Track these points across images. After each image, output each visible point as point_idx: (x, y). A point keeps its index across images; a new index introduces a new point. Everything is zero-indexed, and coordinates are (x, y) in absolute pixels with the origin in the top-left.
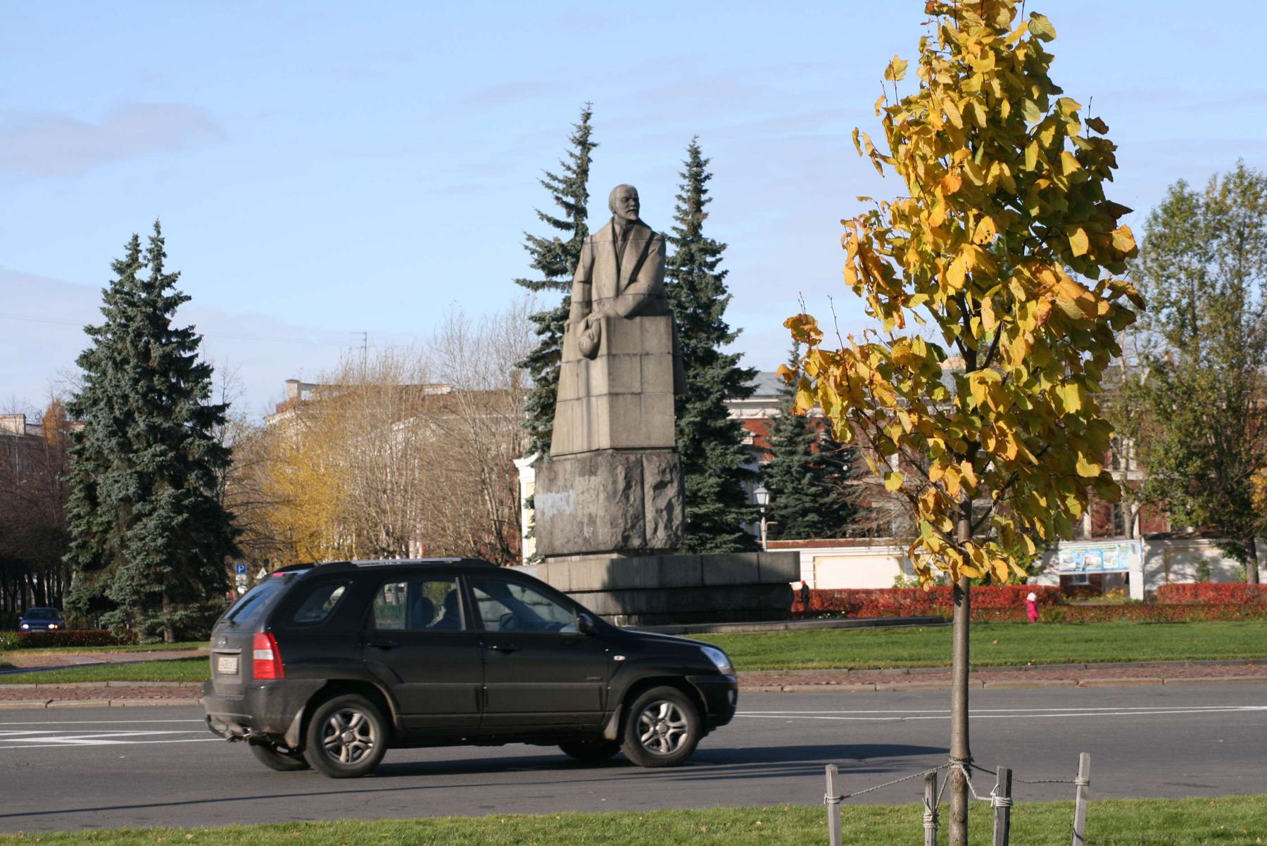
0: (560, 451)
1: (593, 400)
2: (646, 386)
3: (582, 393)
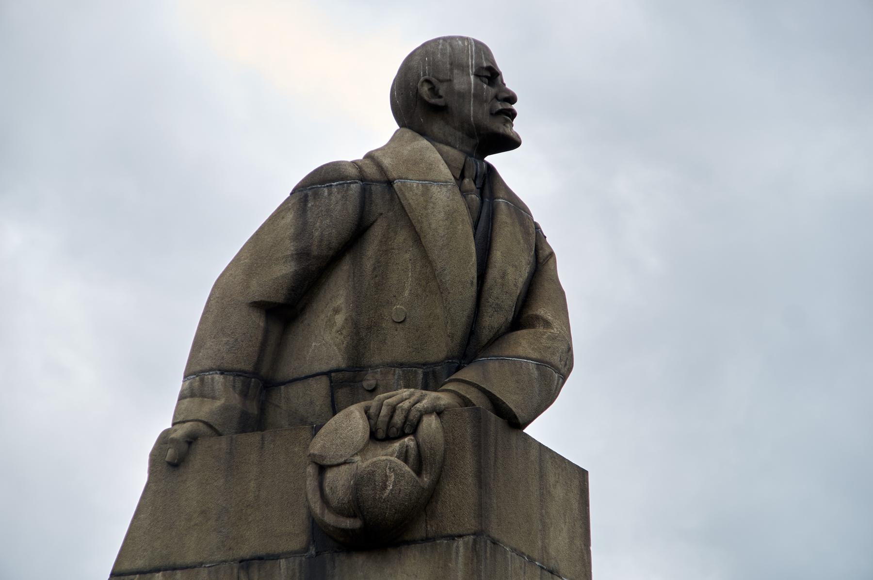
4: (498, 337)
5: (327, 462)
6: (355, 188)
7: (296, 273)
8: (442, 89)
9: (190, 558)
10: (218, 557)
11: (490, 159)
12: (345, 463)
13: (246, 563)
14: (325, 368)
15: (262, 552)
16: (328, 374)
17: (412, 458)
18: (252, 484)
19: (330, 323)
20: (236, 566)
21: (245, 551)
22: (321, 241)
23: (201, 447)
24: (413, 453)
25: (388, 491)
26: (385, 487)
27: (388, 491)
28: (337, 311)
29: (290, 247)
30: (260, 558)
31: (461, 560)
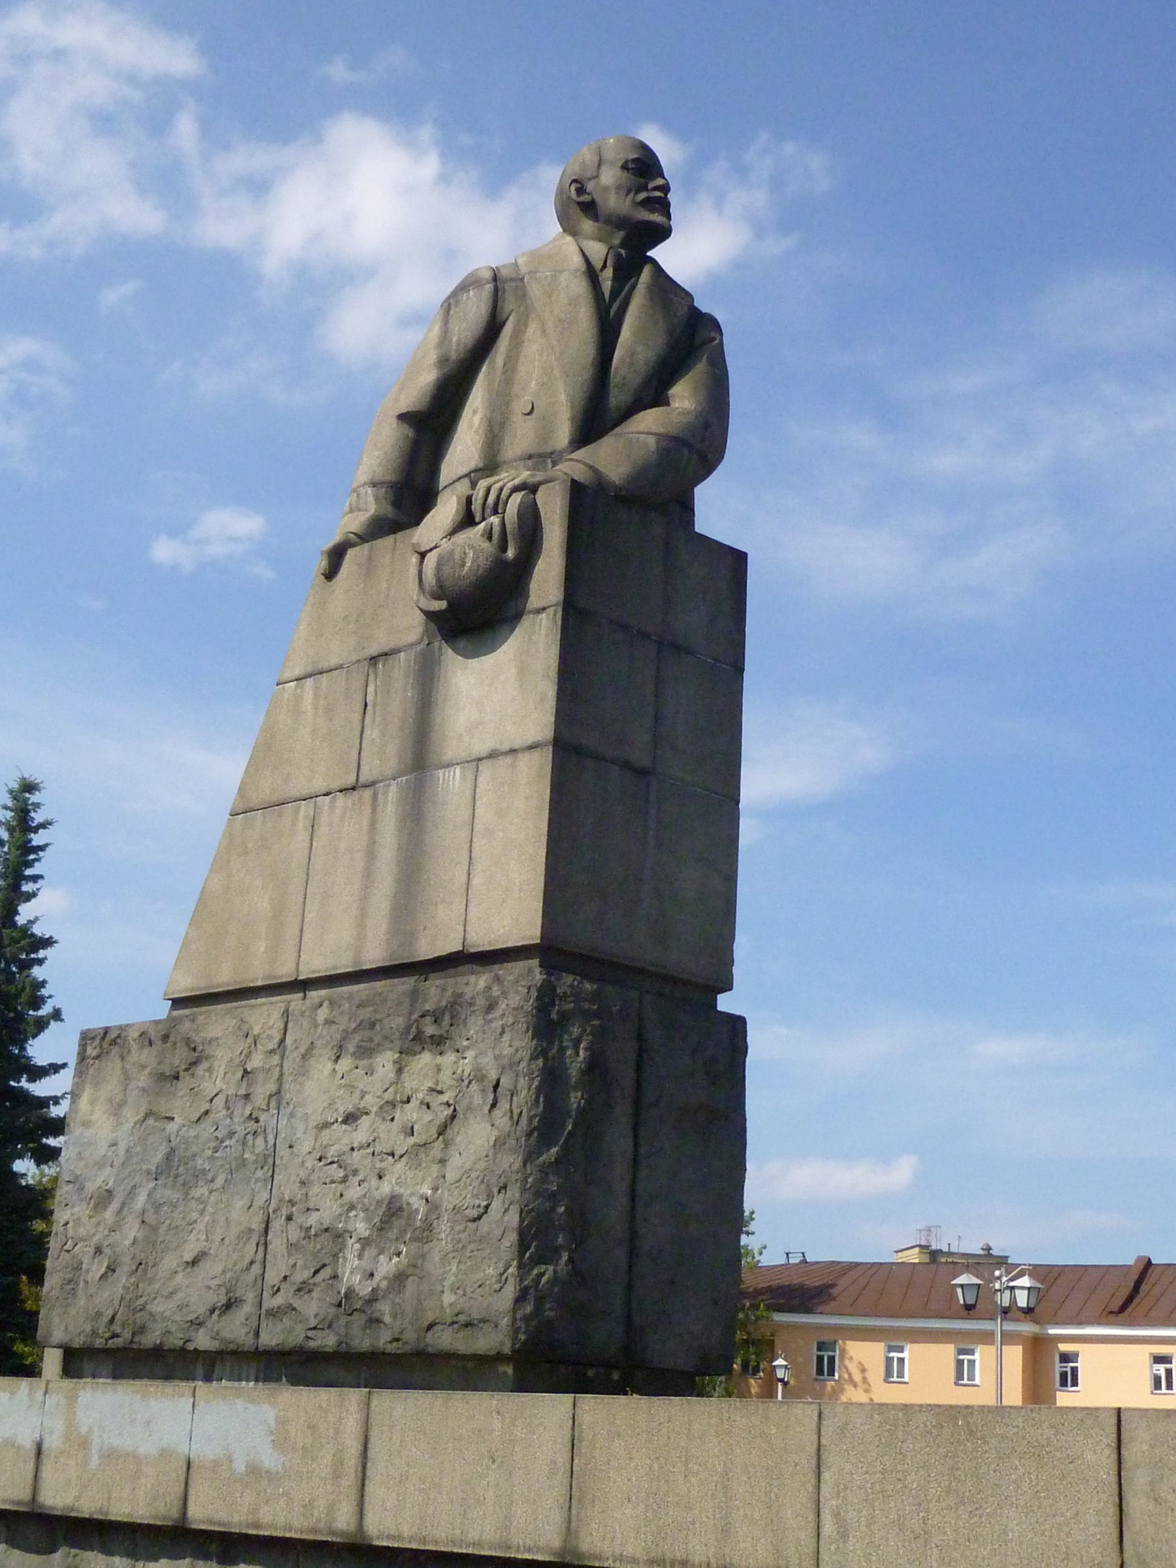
1: (451, 783)
4: (628, 413)
5: (423, 550)
6: (489, 287)
7: (438, 380)
8: (590, 186)
9: (334, 661)
10: (354, 658)
11: (648, 254)
12: (436, 547)
13: (373, 660)
14: (466, 470)
15: (386, 649)
16: (467, 475)
17: (496, 536)
18: (385, 585)
19: (471, 426)
20: (366, 663)
21: (374, 650)
22: (459, 344)
23: (351, 553)
24: (496, 530)
25: (466, 569)
26: (463, 565)
27: (466, 569)
28: (475, 412)
29: (433, 357)
30: (386, 654)
31: (543, 632)
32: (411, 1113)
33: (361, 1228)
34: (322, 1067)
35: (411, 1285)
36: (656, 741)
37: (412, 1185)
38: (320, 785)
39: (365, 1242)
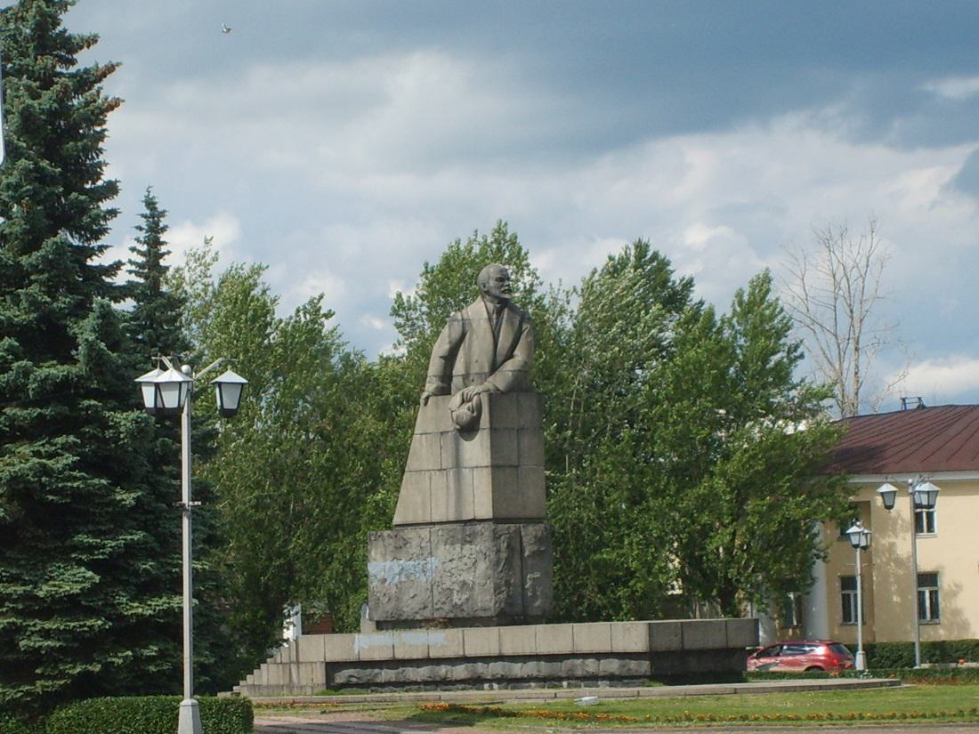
0: (410, 520)
1: (466, 472)
2: (522, 459)
3: (448, 462)
32: (465, 560)
33: (456, 587)
34: (442, 547)
35: (470, 602)
36: (519, 458)
37: (468, 577)
38: (430, 467)
39: (458, 591)
